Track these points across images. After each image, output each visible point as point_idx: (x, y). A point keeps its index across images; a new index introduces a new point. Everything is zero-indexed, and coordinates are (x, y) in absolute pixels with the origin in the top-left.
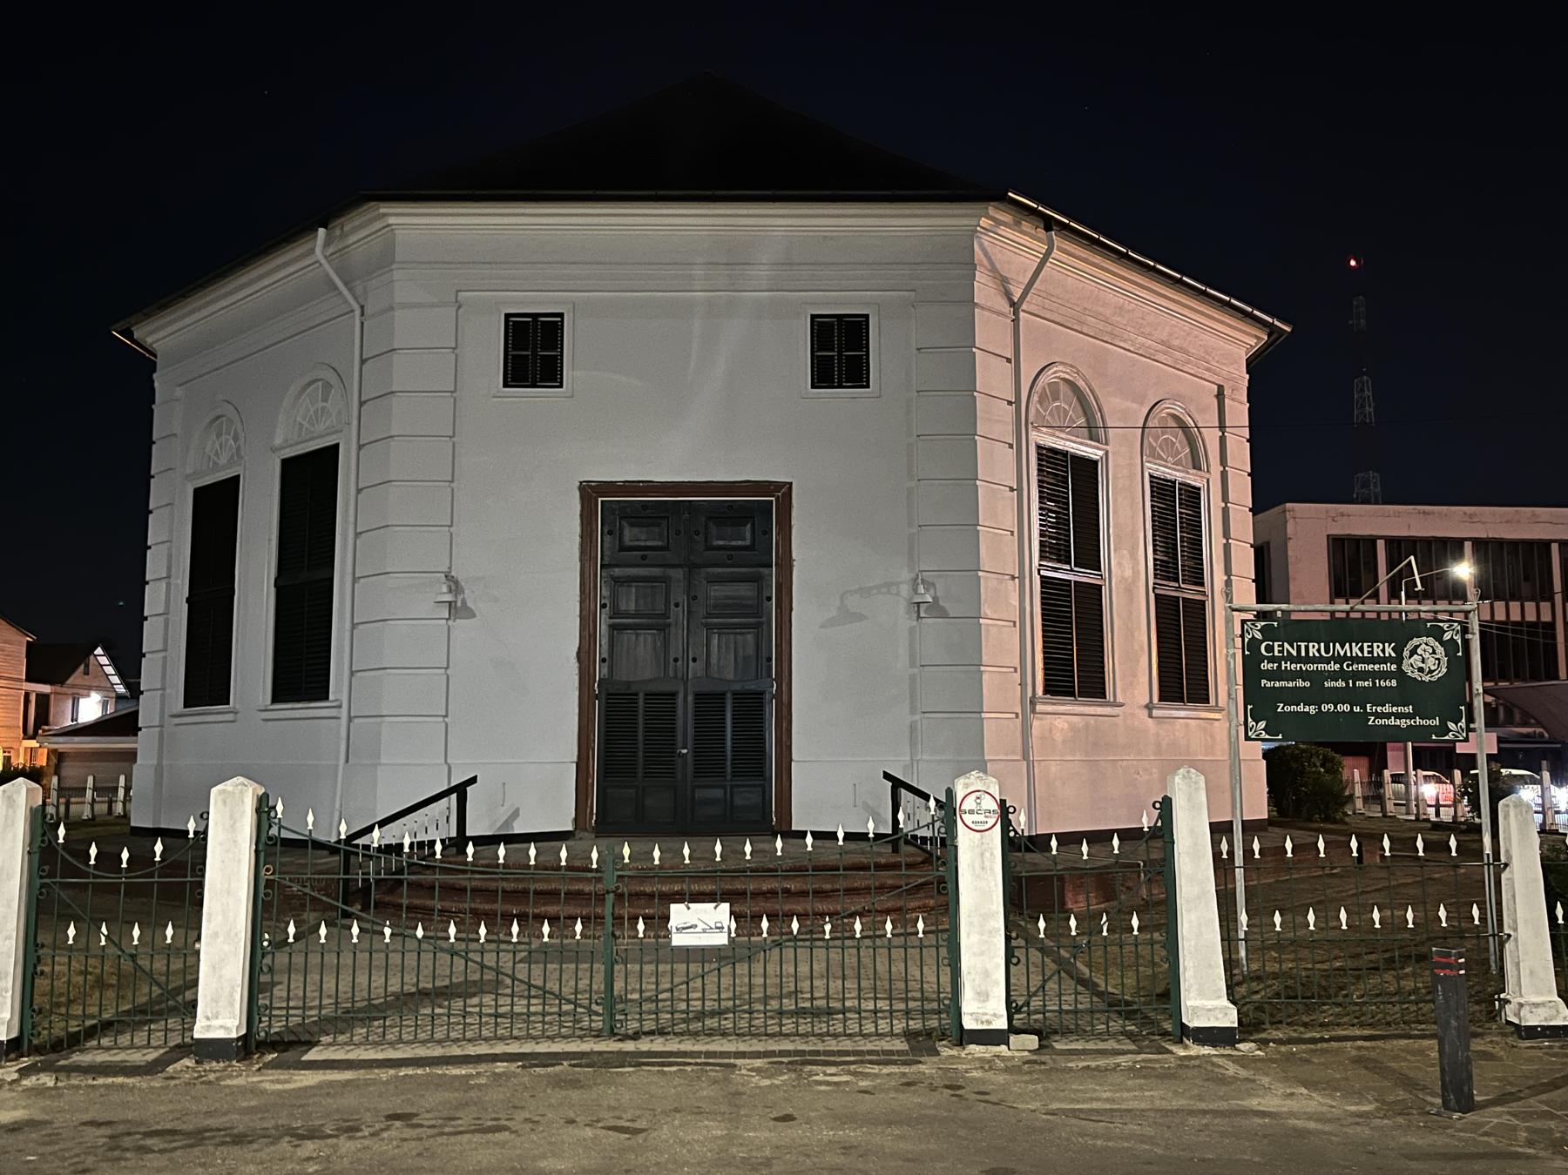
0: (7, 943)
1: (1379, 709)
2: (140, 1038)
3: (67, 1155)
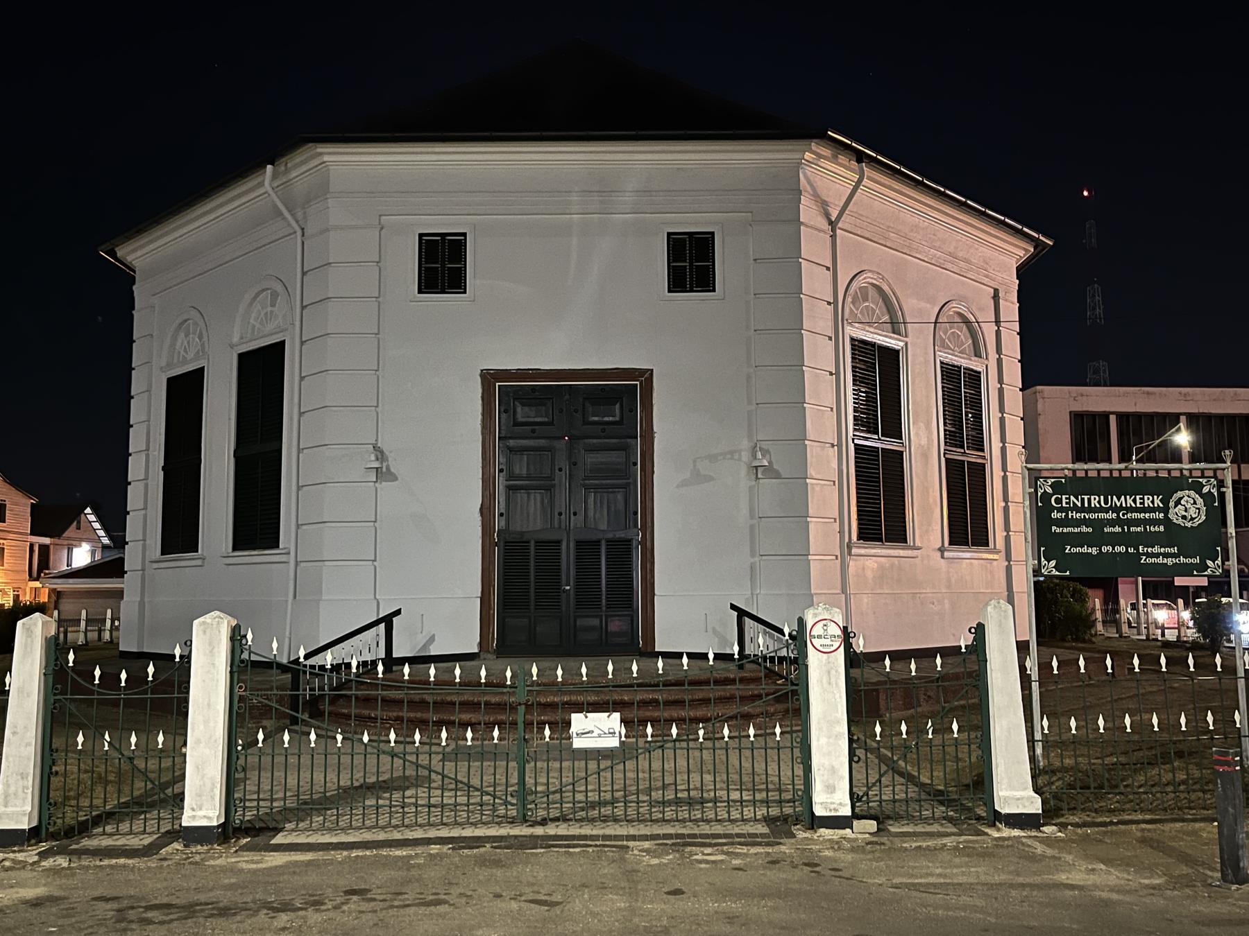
0: (28, 748)
1: (1150, 550)
2: (138, 825)
3: (82, 927)
